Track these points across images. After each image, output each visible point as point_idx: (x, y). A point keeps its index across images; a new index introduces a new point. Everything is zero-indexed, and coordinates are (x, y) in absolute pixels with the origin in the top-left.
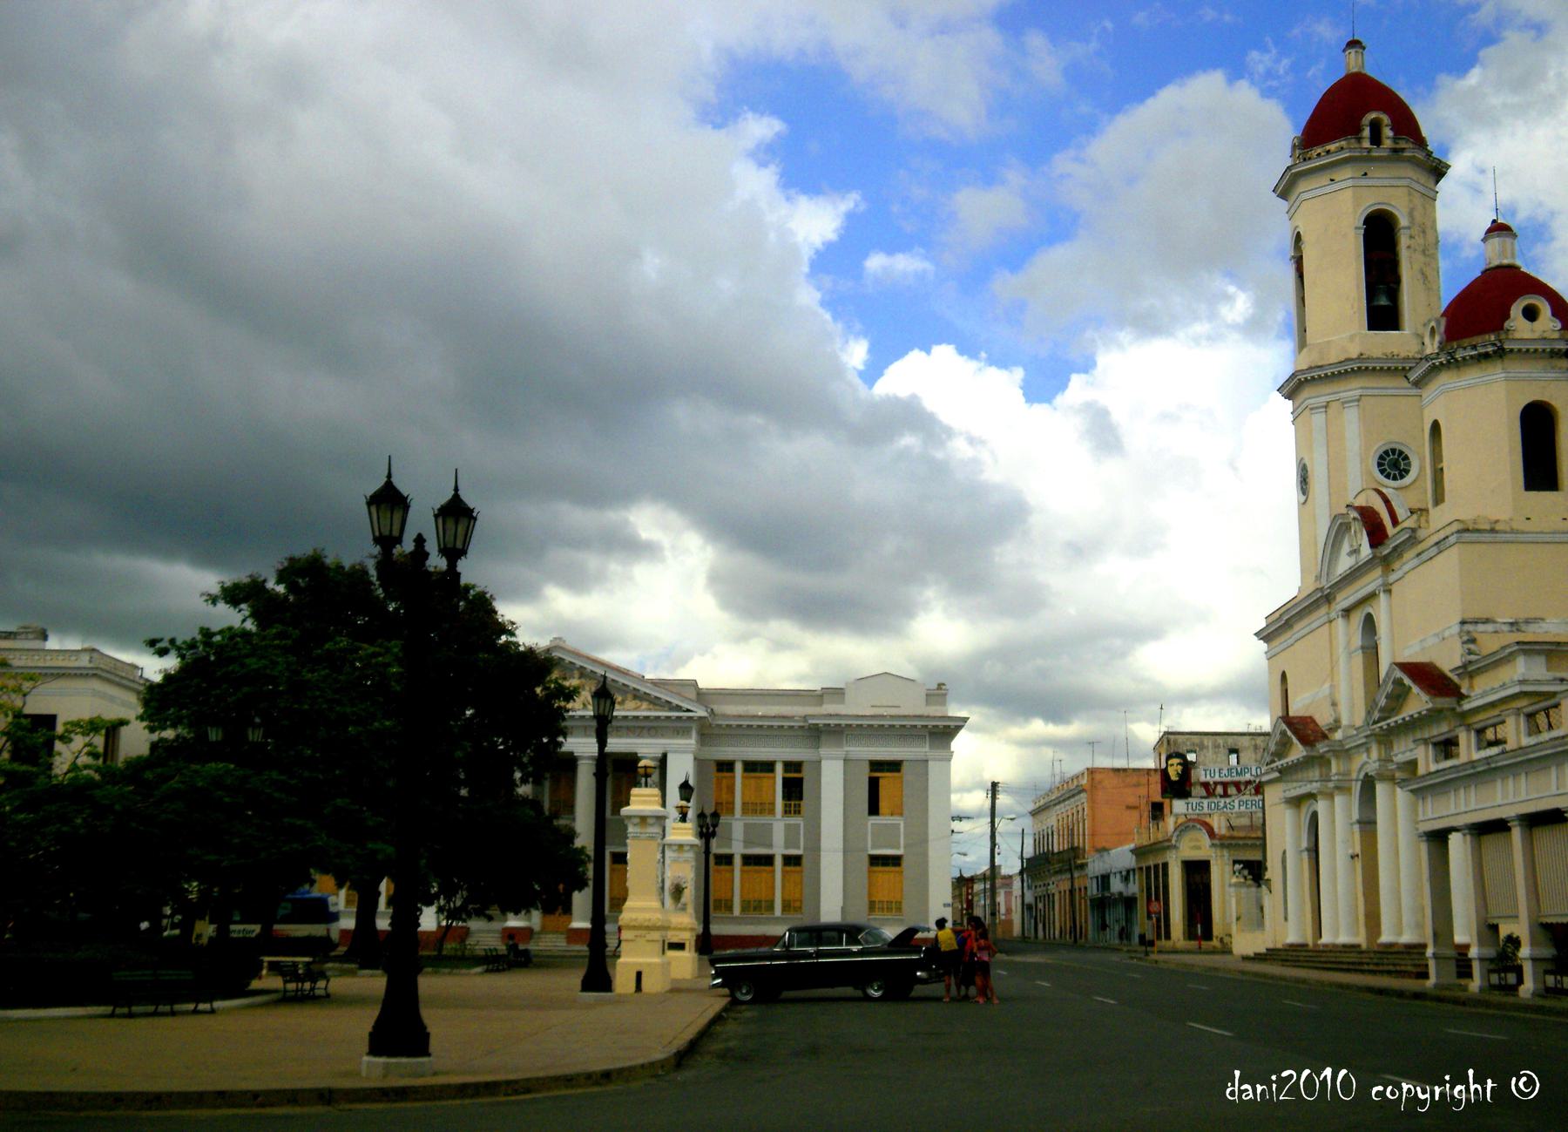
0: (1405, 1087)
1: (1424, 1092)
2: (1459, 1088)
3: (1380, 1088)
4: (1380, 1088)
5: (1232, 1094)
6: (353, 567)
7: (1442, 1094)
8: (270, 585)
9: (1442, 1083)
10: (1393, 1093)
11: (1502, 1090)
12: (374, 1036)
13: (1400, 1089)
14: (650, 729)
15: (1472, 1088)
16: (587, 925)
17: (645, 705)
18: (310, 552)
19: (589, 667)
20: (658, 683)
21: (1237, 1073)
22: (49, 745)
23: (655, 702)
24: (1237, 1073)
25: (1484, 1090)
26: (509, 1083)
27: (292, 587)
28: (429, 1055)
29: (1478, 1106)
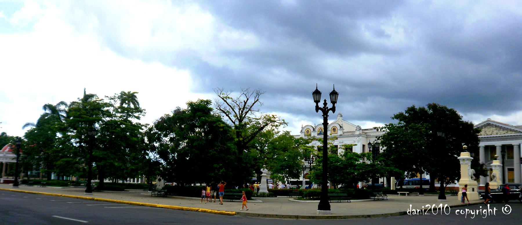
0: (467, 210)
1: (473, 212)
2: (485, 210)
3: (459, 211)
4: (459, 211)
5: (409, 212)
6: (420, 109)
7: (479, 212)
8: (404, 113)
9: (479, 209)
10: (463, 212)
11: (499, 211)
12: (319, 206)
13: (465, 211)
14: (507, 139)
15: (489, 210)
16: (484, 185)
17: (513, 132)
18: (77, 97)
19: (498, 125)
20: (516, 127)
21: (411, 206)
22: (337, 150)
23: (516, 131)
24: (411, 206)
25: (493, 211)
26: (339, 216)
27: (410, 114)
28: (330, 210)
29: (491, 216)
